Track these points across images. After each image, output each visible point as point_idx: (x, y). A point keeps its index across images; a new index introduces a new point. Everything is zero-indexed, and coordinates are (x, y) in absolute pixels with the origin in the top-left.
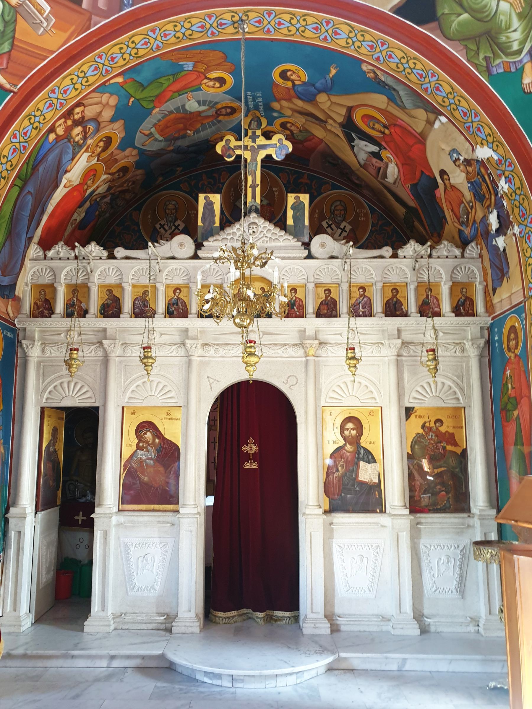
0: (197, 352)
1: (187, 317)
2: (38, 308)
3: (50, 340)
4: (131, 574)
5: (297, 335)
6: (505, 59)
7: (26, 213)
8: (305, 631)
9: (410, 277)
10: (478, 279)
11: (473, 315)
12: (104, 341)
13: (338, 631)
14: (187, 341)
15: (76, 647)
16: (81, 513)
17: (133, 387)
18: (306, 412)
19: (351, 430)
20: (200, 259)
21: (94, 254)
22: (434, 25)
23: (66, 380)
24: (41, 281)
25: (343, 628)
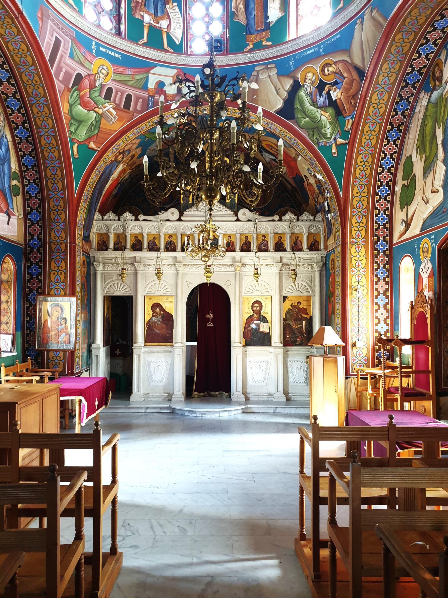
0: (181, 268)
1: (176, 251)
2: (100, 246)
3: (107, 262)
4: (151, 375)
5: (231, 260)
6: (324, 140)
7: (95, 199)
8: (233, 399)
9: (288, 231)
10: (322, 232)
11: (319, 251)
12: (135, 263)
13: (249, 400)
14: (176, 263)
15: (129, 405)
16: (118, 350)
17: (150, 286)
18: (235, 299)
19: (257, 308)
20: (182, 221)
21: (128, 218)
22: (293, 121)
23: (116, 282)
24: (101, 232)
25: (251, 399)
